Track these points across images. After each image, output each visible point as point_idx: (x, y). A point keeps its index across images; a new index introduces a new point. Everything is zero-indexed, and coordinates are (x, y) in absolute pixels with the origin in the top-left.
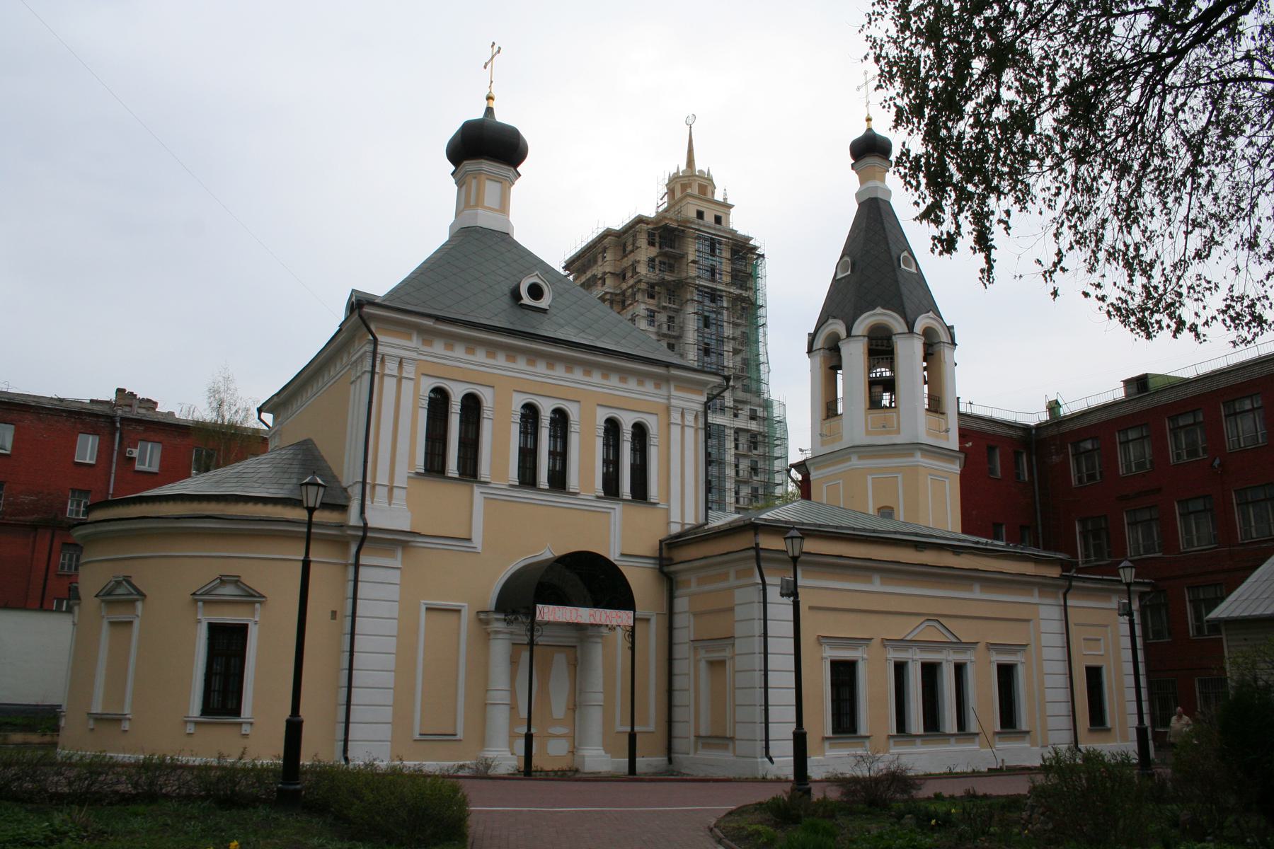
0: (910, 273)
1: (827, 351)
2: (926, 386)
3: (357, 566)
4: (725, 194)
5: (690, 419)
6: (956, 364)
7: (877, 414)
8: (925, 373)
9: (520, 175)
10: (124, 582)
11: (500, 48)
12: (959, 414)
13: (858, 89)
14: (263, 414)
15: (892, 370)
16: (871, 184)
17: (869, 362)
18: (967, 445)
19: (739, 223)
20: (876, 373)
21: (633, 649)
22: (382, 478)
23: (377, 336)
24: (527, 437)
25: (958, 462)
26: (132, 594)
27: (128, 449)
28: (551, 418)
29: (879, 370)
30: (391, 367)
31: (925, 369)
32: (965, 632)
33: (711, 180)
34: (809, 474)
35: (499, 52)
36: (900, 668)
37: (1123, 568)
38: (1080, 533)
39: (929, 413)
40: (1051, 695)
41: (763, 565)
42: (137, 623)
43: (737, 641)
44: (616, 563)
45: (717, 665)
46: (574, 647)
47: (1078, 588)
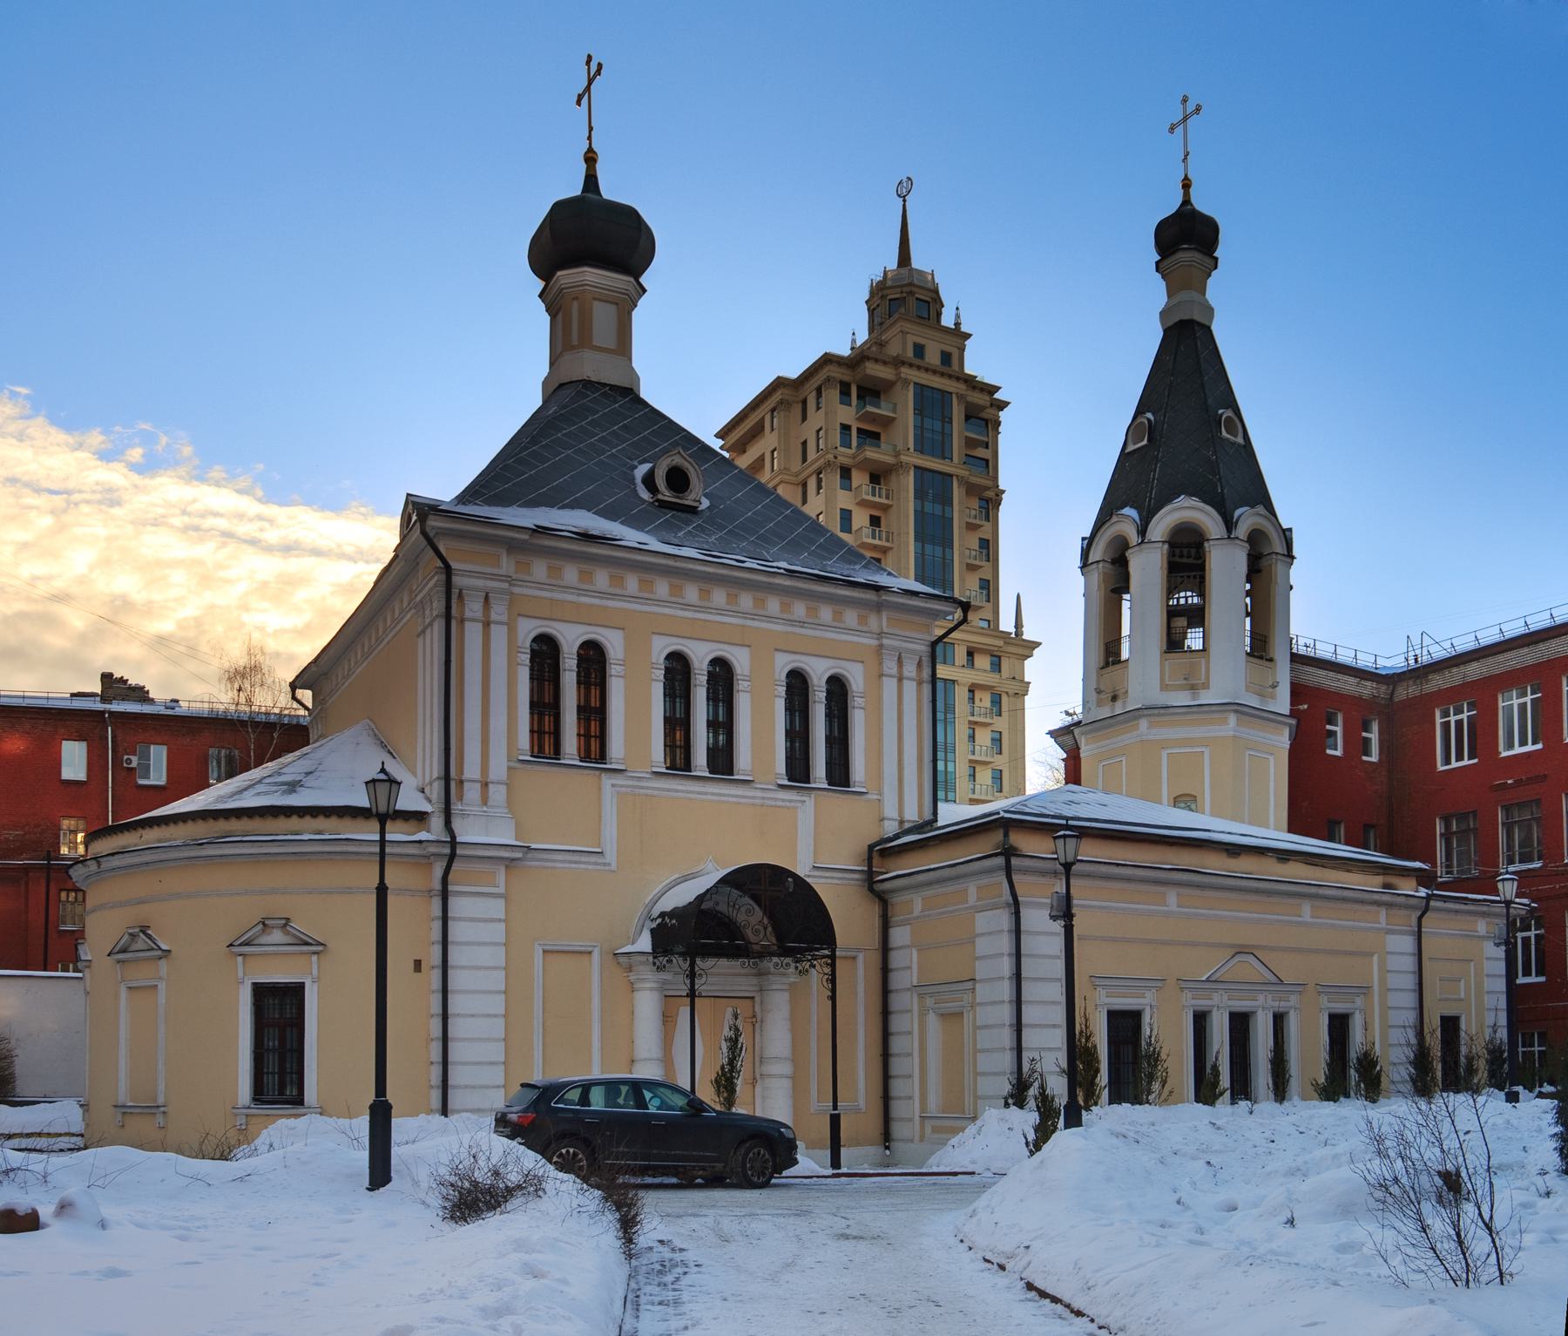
0: (1234, 443)
1: (1108, 565)
3: (445, 895)
4: (958, 316)
5: (910, 669)
6: (1291, 588)
7: (1176, 658)
8: (1248, 600)
9: (644, 291)
10: (141, 935)
11: (600, 66)
12: (1292, 655)
13: (1172, 129)
14: (297, 691)
15: (1202, 595)
16: (1184, 296)
17: (1169, 581)
18: (1301, 707)
20: (1178, 599)
21: (833, 998)
22: (472, 769)
23: (451, 563)
24: (674, 703)
25: (1286, 732)
26: (153, 949)
27: (126, 757)
28: (709, 672)
29: (1182, 594)
30: (474, 608)
31: (1248, 593)
32: (1289, 968)
33: (937, 292)
34: (1078, 748)
35: (599, 72)
37: (1503, 880)
38: (1441, 835)
39: (1251, 659)
40: (1489, 984)
41: (1015, 877)
42: (162, 986)
43: (978, 986)
45: (952, 1017)
46: (752, 998)
47: (1438, 910)
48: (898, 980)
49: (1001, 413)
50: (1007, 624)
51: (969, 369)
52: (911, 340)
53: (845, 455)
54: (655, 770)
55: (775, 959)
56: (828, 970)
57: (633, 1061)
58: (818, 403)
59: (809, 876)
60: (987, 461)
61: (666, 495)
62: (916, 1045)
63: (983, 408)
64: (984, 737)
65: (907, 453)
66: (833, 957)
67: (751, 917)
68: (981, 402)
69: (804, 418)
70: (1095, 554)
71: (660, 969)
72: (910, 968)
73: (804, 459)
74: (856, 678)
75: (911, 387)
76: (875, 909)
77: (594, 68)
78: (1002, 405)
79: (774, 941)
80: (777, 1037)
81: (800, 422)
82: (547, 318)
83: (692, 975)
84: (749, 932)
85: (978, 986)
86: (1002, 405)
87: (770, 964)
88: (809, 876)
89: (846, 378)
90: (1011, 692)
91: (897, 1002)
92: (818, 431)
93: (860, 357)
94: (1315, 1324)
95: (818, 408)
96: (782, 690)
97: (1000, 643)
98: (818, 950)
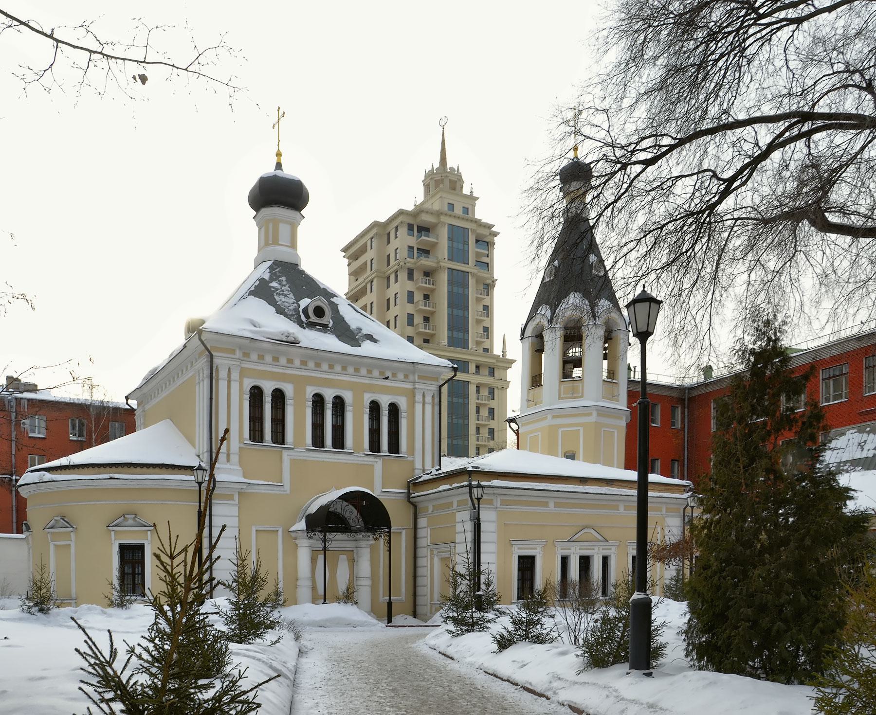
2: (605, 362)
10: (61, 520)
17: (563, 347)
18: (633, 405)
19: (481, 213)
21: (390, 551)
23: (213, 353)
24: (317, 416)
36: (565, 560)
44: (378, 497)
48: (422, 542)
49: (495, 238)
50: (497, 351)
51: (477, 216)
52: (446, 201)
53: (411, 263)
54: (308, 448)
55: (363, 533)
56: (387, 538)
57: (297, 579)
58: (396, 235)
59: (379, 495)
60: (488, 264)
61: (314, 319)
62: (429, 572)
63: (486, 236)
64: (484, 412)
65: (444, 261)
66: (390, 532)
67: (351, 513)
68: (485, 233)
69: (389, 243)
70: (528, 333)
71: (310, 538)
72: (427, 537)
73: (388, 264)
74: (403, 403)
75: (447, 226)
76: (411, 509)
77: (281, 114)
78: (496, 234)
79: (363, 525)
80: (364, 567)
81: (386, 244)
82: (257, 229)
83: (325, 541)
84: (351, 522)
85: (457, 545)
86: (496, 234)
87: (359, 536)
88: (379, 495)
89: (411, 222)
90: (500, 387)
91: (421, 552)
92: (396, 250)
93: (419, 211)
94: (525, 665)
95: (396, 237)
96: (368, 410)
97: (494, 361)
98: (383, 529)
